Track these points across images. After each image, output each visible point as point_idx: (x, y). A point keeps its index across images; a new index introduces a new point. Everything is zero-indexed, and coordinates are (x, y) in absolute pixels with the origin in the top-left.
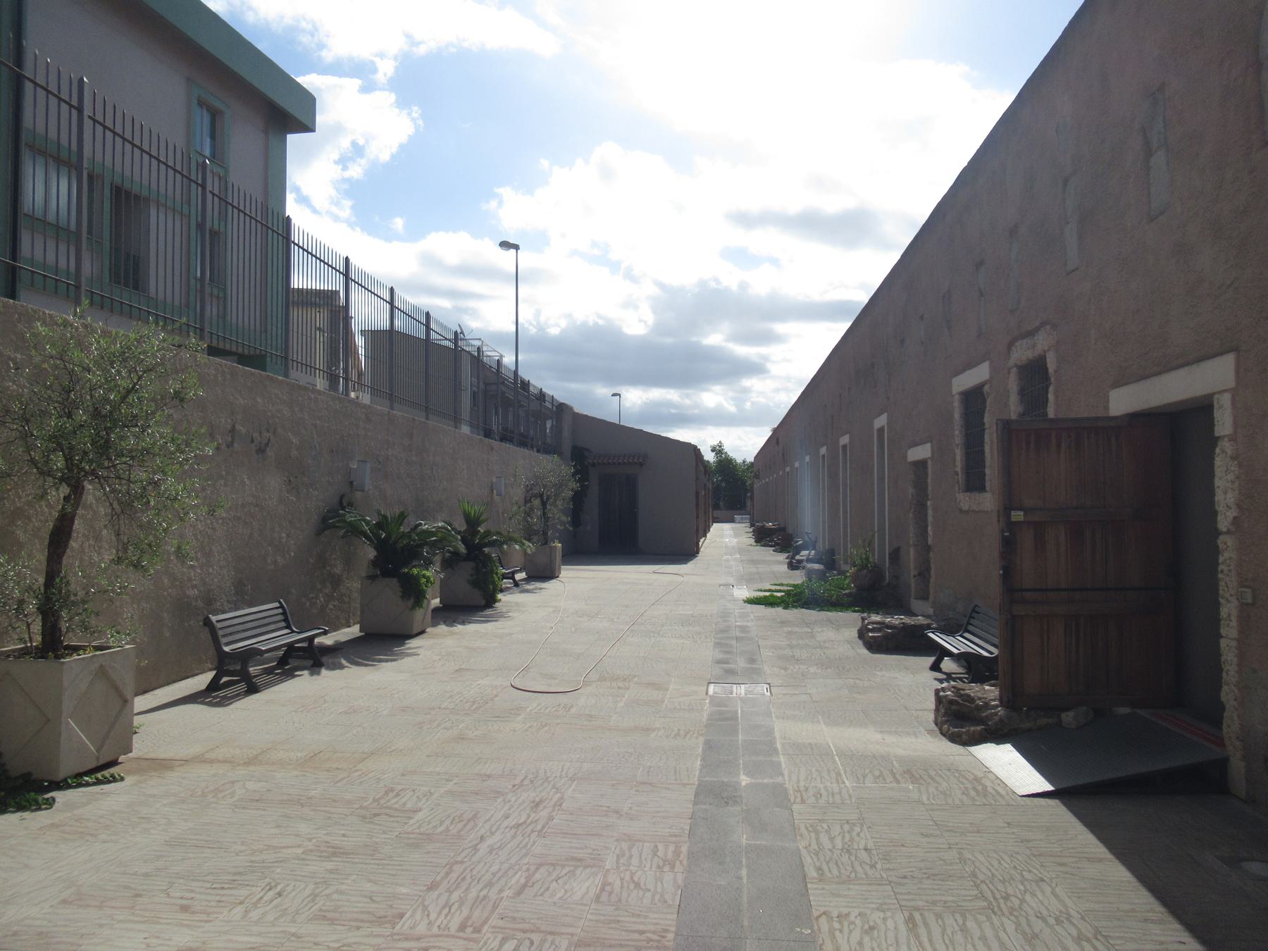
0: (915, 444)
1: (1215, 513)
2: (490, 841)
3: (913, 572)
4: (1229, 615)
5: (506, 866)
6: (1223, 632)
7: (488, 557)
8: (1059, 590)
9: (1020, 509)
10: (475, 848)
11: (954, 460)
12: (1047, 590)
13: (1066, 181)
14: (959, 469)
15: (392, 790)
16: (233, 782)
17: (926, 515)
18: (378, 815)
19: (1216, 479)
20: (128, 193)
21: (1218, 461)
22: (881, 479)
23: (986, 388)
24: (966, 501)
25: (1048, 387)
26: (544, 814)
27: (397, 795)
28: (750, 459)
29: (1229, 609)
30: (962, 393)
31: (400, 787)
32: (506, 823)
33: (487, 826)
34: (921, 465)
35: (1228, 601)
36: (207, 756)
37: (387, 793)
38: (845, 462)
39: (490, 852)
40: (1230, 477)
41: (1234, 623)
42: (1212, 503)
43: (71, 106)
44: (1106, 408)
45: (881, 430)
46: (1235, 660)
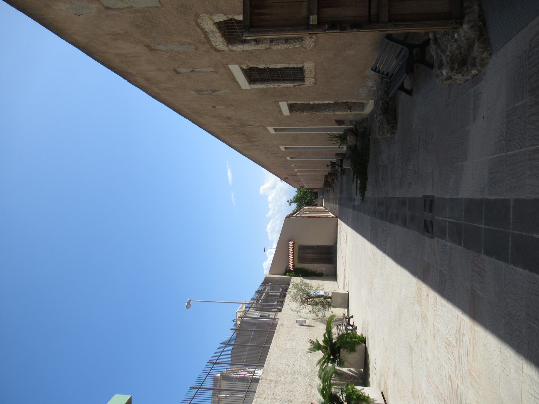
0: (280, 112)
3: (349, 113)
7: (341, 337)
9: (308, 19)
11: (287, 88)
22: (300, 130)
23: (244, 67)
24: (309, 81)
28: (296, 189)
30: (250, 84)
34: (292, 107)
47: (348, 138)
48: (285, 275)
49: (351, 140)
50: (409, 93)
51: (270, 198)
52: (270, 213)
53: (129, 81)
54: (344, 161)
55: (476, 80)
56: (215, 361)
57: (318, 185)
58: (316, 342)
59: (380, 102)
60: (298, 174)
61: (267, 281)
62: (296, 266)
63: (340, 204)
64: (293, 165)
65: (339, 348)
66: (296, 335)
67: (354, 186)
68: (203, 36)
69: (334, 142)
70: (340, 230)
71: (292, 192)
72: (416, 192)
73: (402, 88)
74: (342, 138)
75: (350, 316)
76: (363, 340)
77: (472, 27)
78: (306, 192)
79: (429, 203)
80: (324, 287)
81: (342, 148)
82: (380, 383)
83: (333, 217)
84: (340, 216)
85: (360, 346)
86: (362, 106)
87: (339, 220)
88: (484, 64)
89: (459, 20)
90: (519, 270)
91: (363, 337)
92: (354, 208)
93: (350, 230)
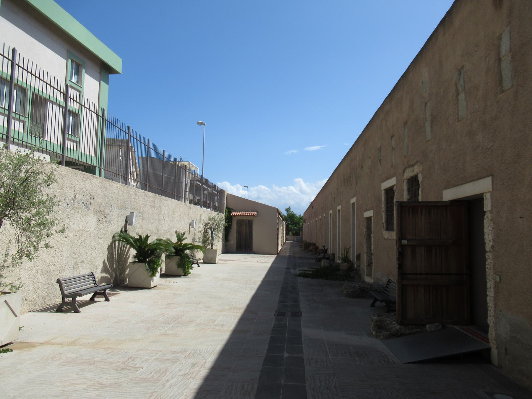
1: (484, 243)
2: (171, 382)
3: (366, 264)
4: (491, 287)
5: (176, 393)
6: (488, 293)
8: (422, 274)
9: (406, 240)
10: (164, 385)
11: (382, 217)
12: (416, 274)
13: (426, 104)
14: (384, 221)
15: (131, 358)
16: (61, 354)
17: (371, 240)
18: (123, 369)
19: (485, 229)
20: (41, 97)
21: (485, 221)
23: (395, 188)
24: (386, 234)
25: (419, 188)
26: (197, 369)
27: (133, 360)
28: (302, 215)
29: (490, 284)
31: (135, 356)
32: (180, 373)
33: (171, 375)
34: (369, 219)
35: (490, 280)
36: (54, 341)
37: (129, 359)
38: (339, 217)
39: (170, 387)
40: (490, 228)
41: (492, 290)
42: (483, 239)
43: (9, 60)
44: (442, 198)
45: (353, 204)
46: (493, 306)
47: (346, 264)
48: (226, 208)
49: (344, 266)
50: (373, 305)
51: (292, 188)
52: (277, 189)
53: (387, 98)
54: (328, 261)
55: (370, 335)
56: (150, 146)
57: (306, 236)
58: (184, 237)
59: (369, 287)
60: (317, 219)
61: (222, 192)
62: (234, 217)
63: (290, 257)
64: (324, 215)
65: (180, 255)
66: (170, 219)
67: (306, 269)
68: (412, 164)
69: (343, 252)
70: (267, 257)
71: (300, 210)
72: (304, 307)
73: (376, 300)
74: (346, 259)
75: (200, 265)
76: (186, 274)
77: (397, 330)
78: (299, 224)
79: (297, 314)
80: (218, 245)
81: (339, 259)
82: (161, 285)
83: (278, 250)
84: (486, 252)
85: (182, 271)
86: (369, 275)
87: (276, 256)
88: (377, 337)
89: (401, 323)
90: (267, 347)
91: (188, 274)
92: (288, 268)
93: (269, 265)
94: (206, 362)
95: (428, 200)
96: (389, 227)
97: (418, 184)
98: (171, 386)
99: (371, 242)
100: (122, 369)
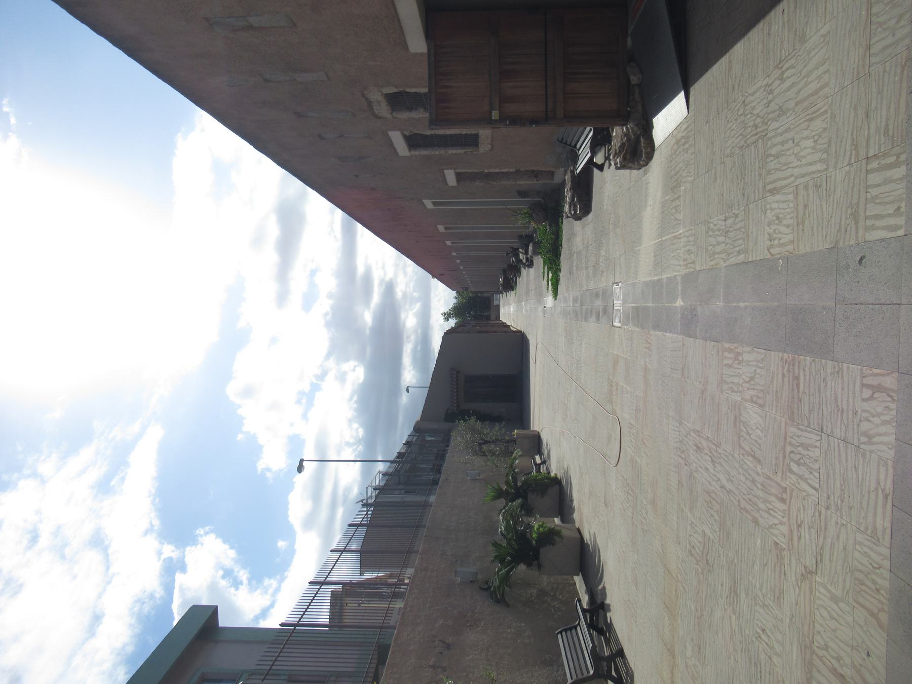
2: (724, 481)
3: (535, 182)
5: (741, 470)
7: (524, 483)
9: (491, 113)
10: (729, 492)
12: (546, 94)
13: (266, 81)
14: (463, 151)
22: (470, 203)
23: (407, 133)
28: (454, 293)
30: (410, 150)
32: (712, 470)
33: (714, 483)
34: (459, 177)
37: (692, 555)
39: (732, 481)
44: (422, 54)
45: (434, 204)
60: (462, 268)
64: (454, 254)
94: (693, 431)
95: (427, 76)
96: (472, 141)
97: (400, 94)
98: (730, 480)
99: (498, 173)
100: (708, 563)
